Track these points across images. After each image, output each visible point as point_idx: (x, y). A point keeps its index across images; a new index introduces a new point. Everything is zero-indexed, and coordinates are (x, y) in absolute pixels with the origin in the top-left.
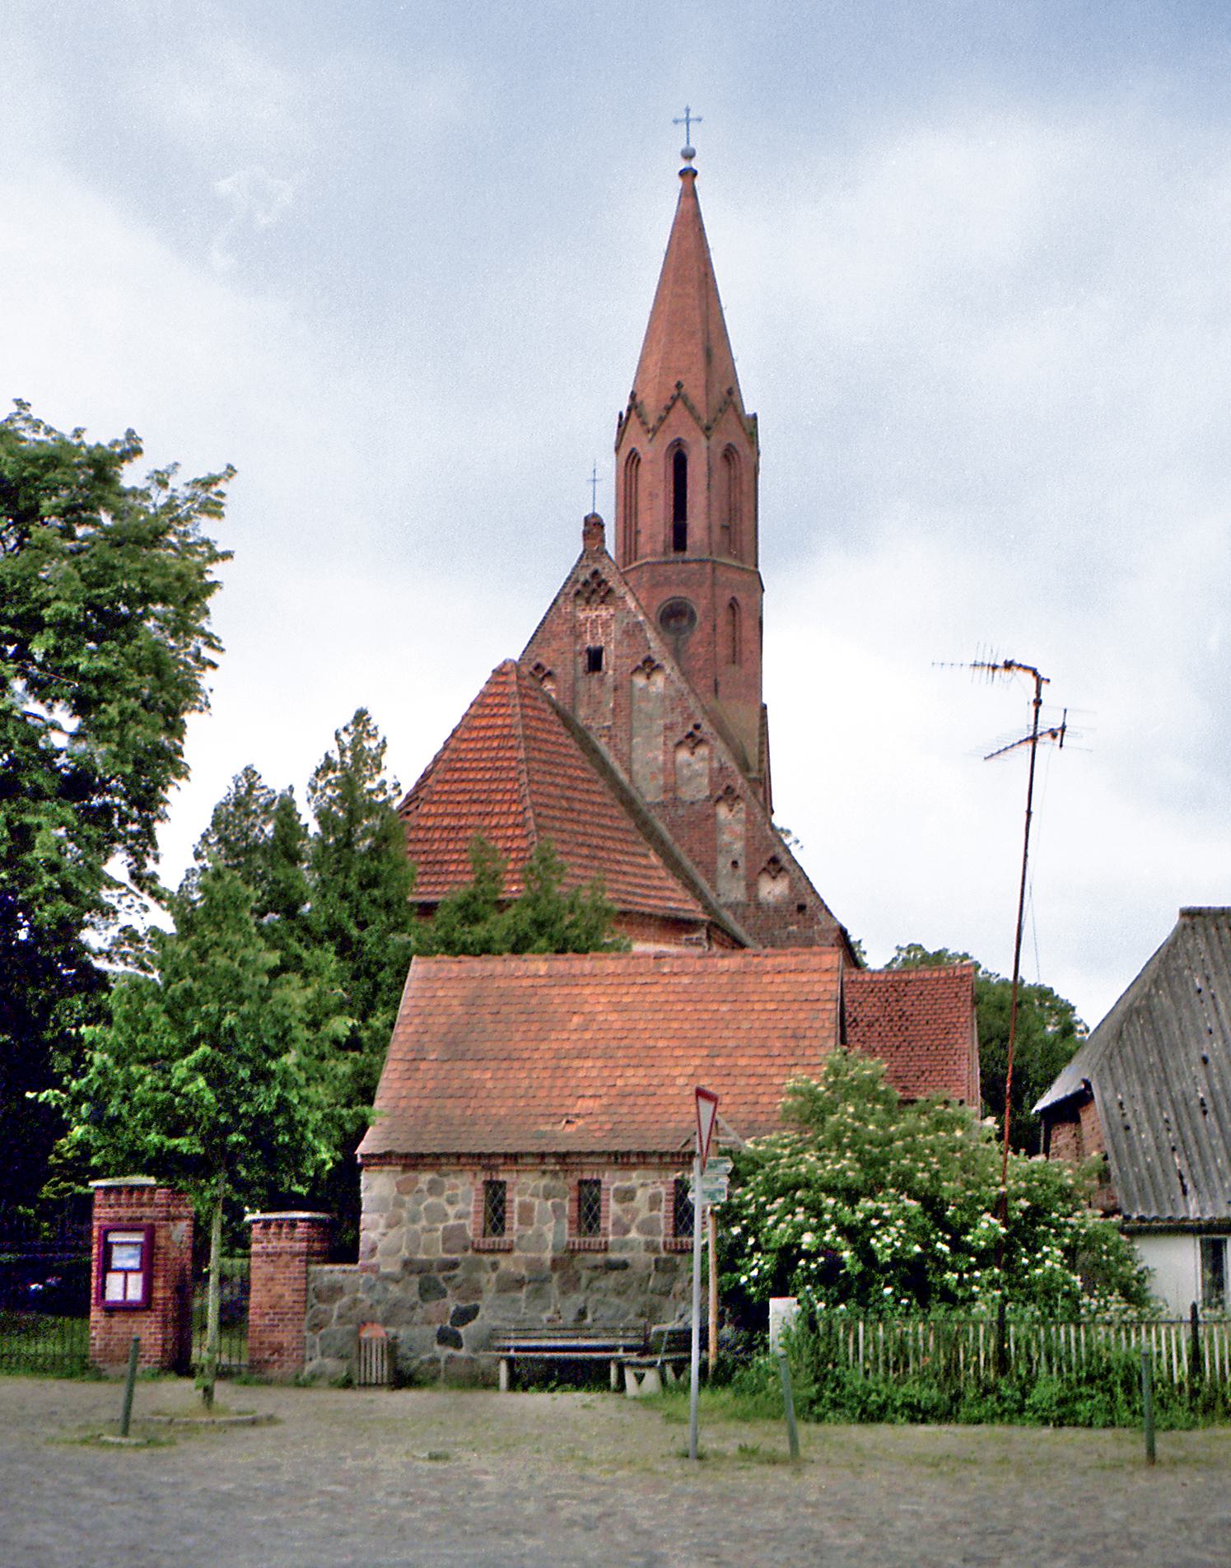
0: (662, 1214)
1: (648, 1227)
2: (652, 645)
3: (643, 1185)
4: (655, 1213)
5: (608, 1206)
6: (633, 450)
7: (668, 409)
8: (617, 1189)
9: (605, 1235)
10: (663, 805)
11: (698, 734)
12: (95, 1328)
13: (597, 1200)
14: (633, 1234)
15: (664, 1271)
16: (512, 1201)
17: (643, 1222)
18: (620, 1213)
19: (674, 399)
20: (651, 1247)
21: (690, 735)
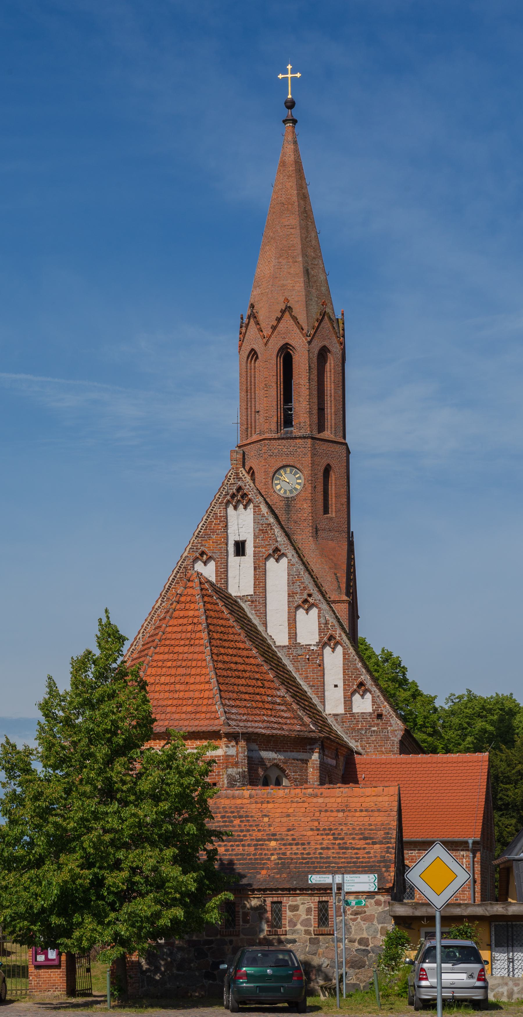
0: (312, 917)
1: (306, 923)
2: (279, 539)
3: (303, 904)
4: (309, 917)
5: (286, 914)
6: (252, 350)
7: (279, 320)
8: (290, 906)
9: (286, 927)
10: (288, 647)
11: (310, 600)
12: (32, 975)
13: (280, 910)
14: (299, 927)
15: (314, 944)
16: (239, 912)
17: (303, 920)
18: (292, 917)
19: (283, 312)
20: (307, 932)
21: (306, 601)
